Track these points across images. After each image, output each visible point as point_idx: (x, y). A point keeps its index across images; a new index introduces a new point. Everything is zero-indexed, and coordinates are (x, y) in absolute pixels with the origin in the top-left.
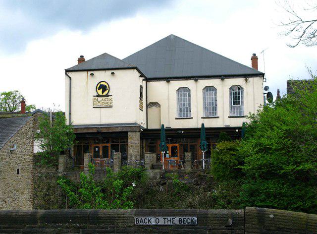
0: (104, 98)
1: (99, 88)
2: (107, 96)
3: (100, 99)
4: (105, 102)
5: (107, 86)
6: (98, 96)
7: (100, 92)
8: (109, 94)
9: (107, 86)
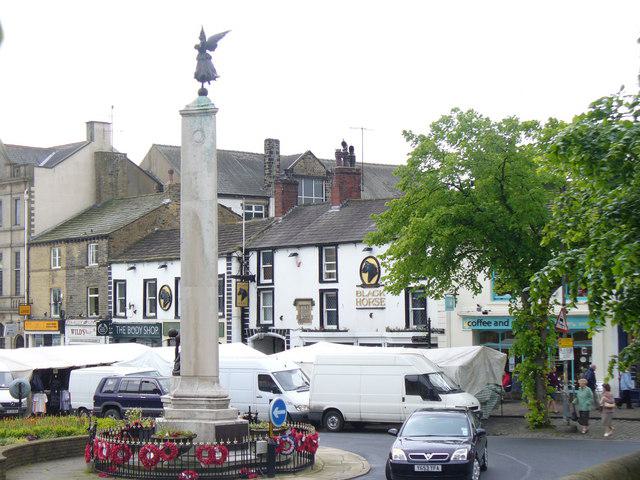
0: (372, 290)
3: (367, 291)
6: (364, 286)
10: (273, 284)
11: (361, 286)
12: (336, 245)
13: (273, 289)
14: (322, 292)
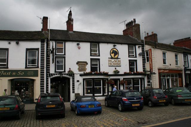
0: (115, 60)
1: (112, 53)
2: (117, 58)
3: (113, 60)
4: (116, 62)
5: (117, 51)
6: (112, 58)
7: (113, 55)
8: (119, 57)
9: (117, 51)
10: (65, 54)
11: (111, 58)
12: (99, 43)
13: (65, 58)
14: (91, 59)
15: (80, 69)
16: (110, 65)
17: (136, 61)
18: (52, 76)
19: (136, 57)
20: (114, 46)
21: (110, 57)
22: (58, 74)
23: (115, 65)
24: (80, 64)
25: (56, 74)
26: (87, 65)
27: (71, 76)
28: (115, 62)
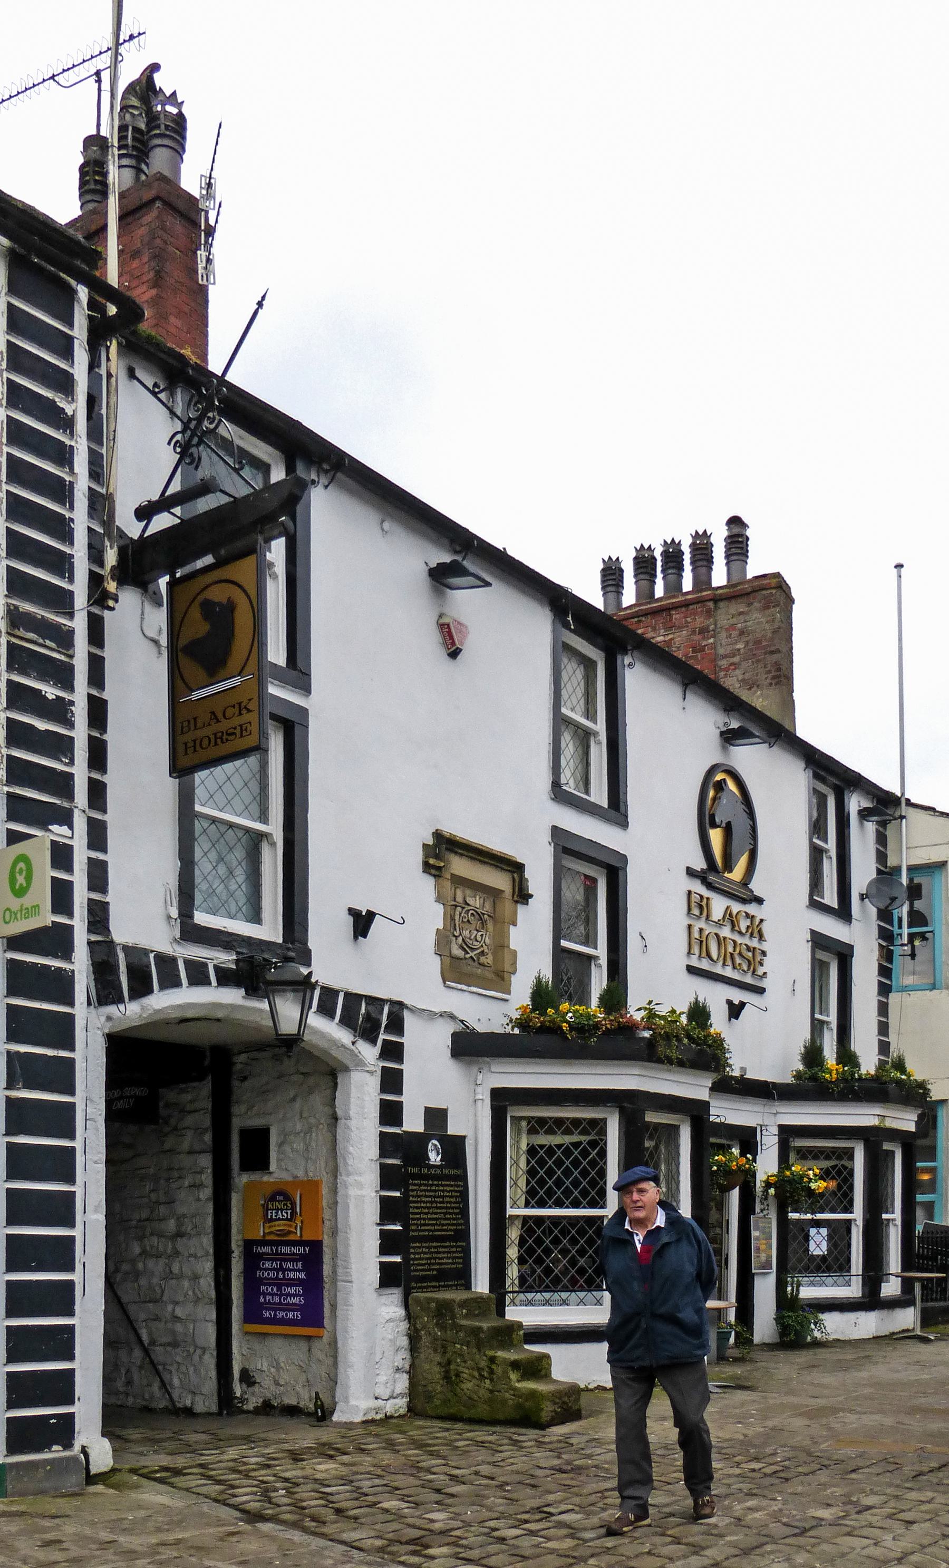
0: (736, 907)
3: (719, 905)
4: (739, 940)
15: (457, 952)
16: (695, 962)
17: (844, 955)
18: (141, 988)
19: (843, 913)
20: (729, 737)
21: (700, 864)
22: (226, 978)
23: (729, 972)
24: (460, 881)
25: (198, 975)
26: (521, 909)
27: (369, 1034)
28: (726, 932)
